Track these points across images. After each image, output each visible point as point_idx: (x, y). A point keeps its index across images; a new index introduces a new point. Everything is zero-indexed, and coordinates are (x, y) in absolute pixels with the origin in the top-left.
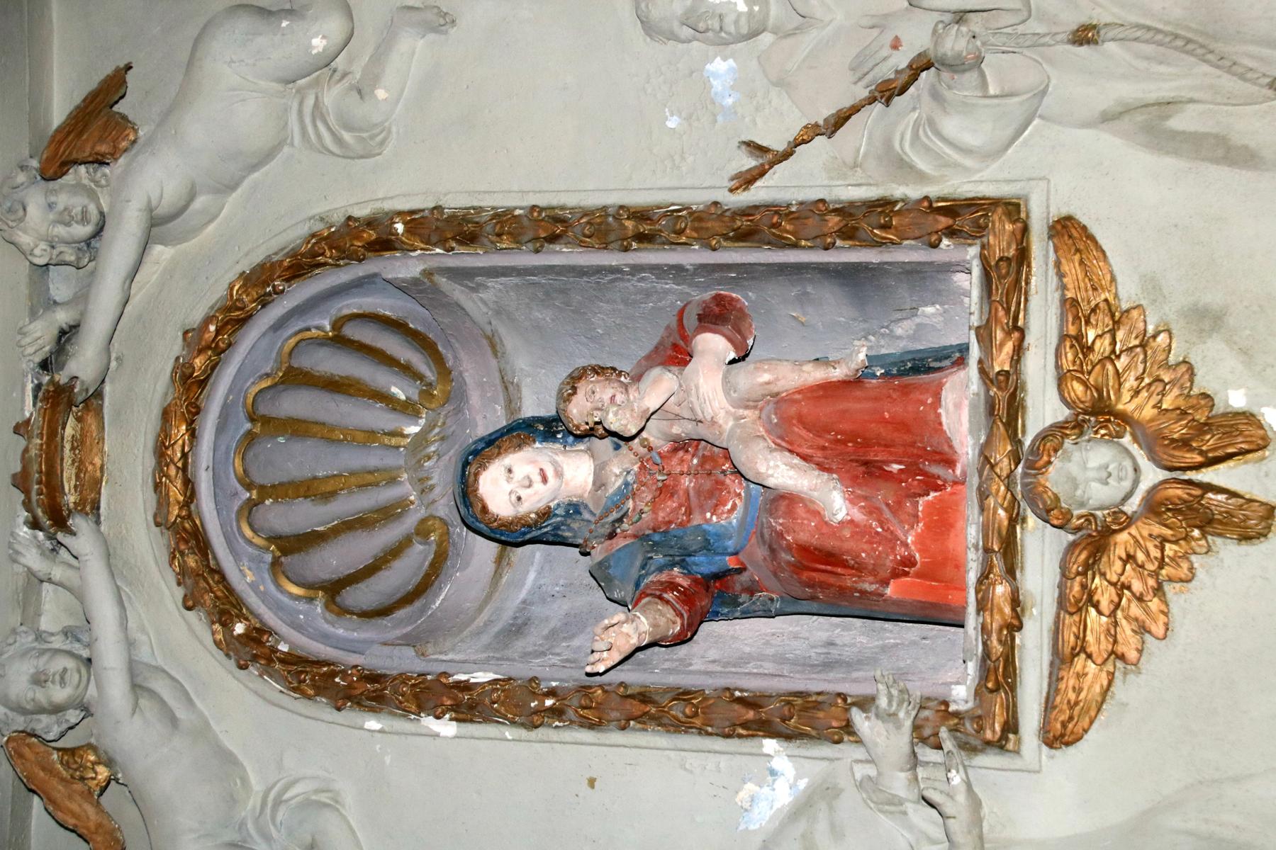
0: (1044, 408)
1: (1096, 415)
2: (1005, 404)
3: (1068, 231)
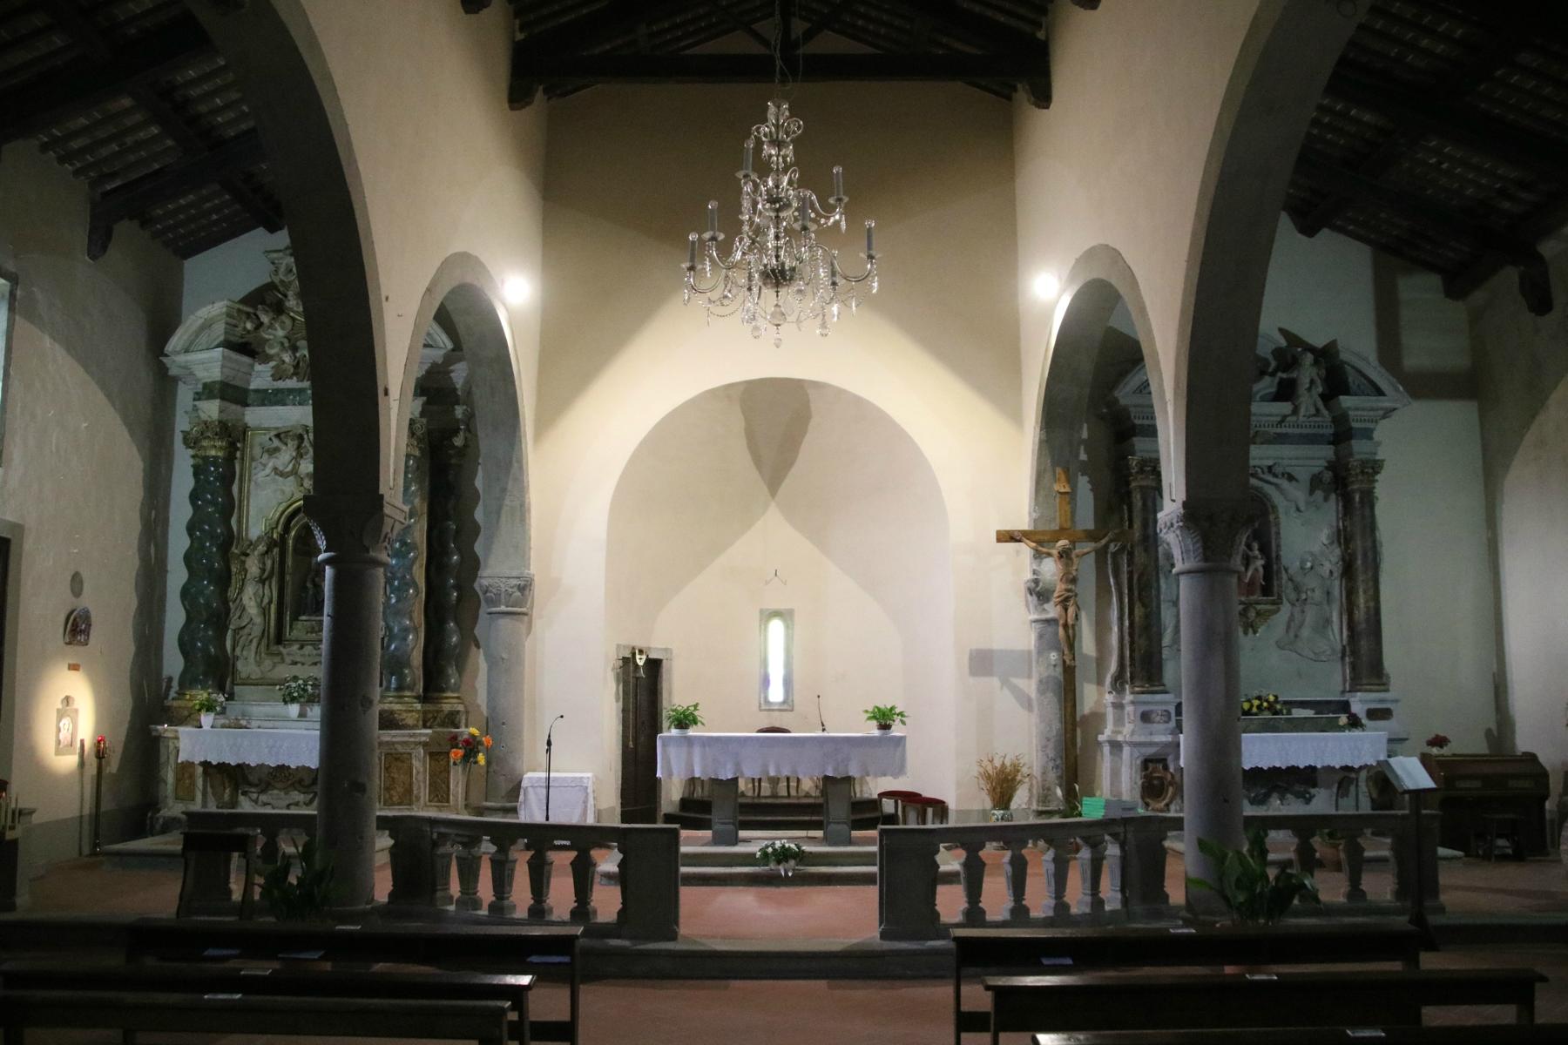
1: (1258, 614)
2: (1258, 603)
3: (1278, 611)
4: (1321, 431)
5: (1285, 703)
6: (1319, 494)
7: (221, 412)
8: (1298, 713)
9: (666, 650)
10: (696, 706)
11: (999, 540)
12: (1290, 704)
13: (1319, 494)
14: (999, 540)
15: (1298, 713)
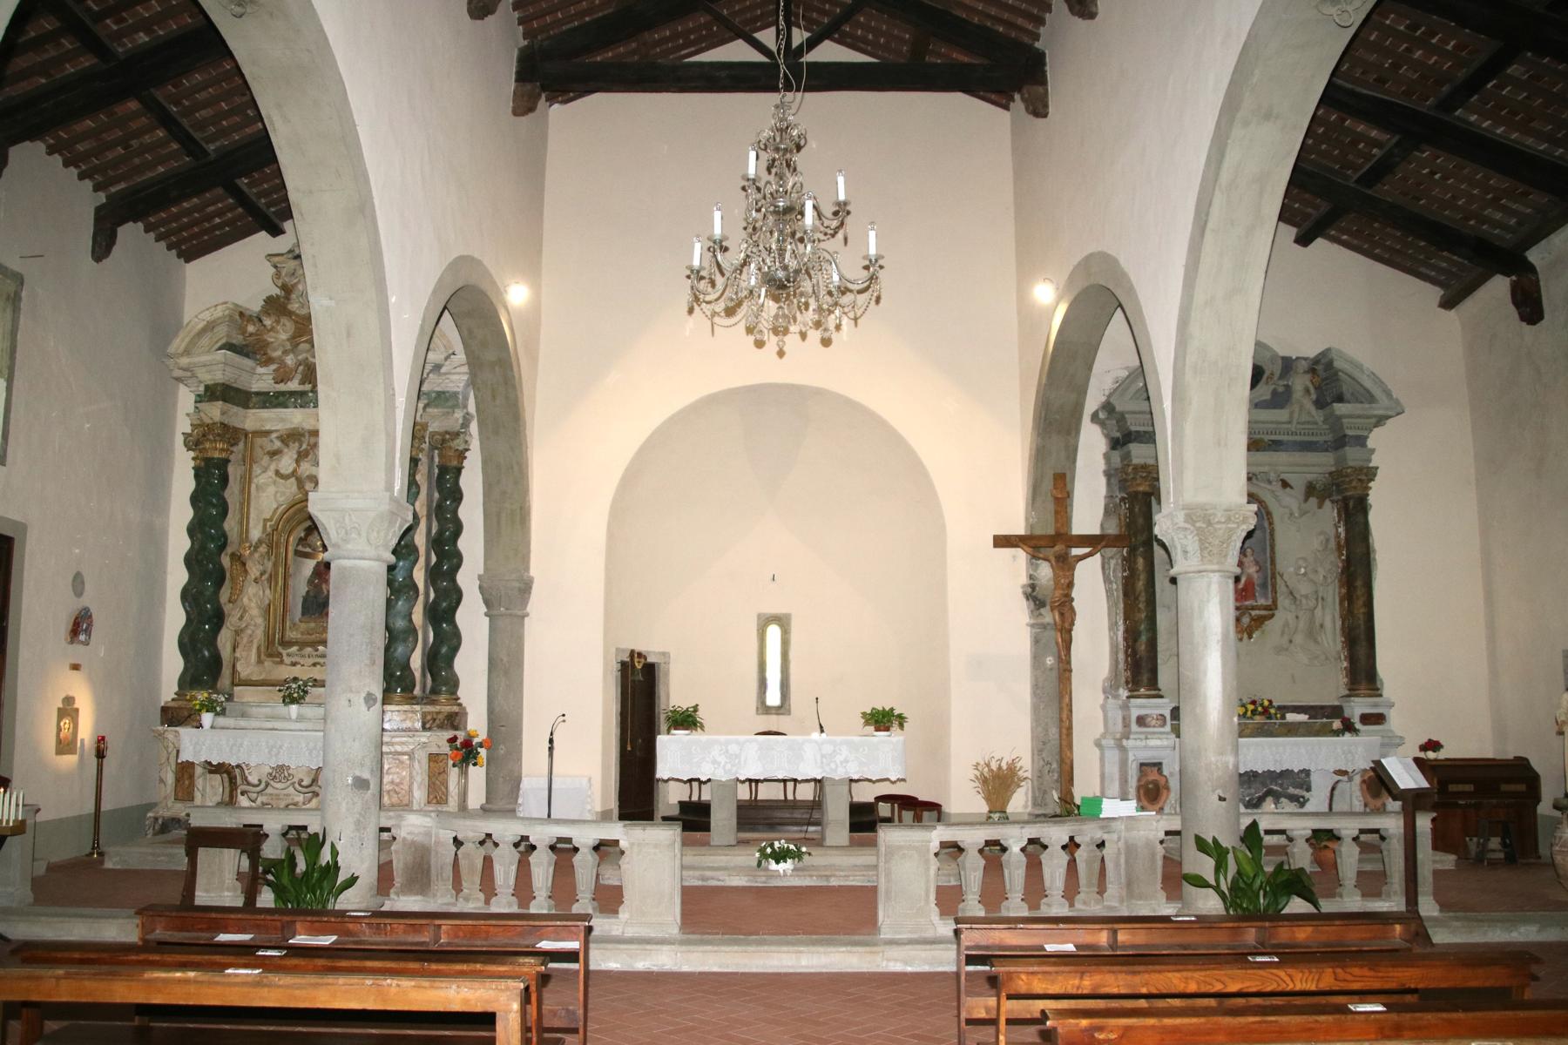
0: (1253, 613)
2: (1253, 608)
4: (1314, 439)
5: (1279, 708)
6: (1313, 501)
7: (223, 413)
8: (1291, 717)
9: (664, 654)
10: (696, 708)
11: (996, 545)
12: (1284, 709)
13: (1313, 501)
14: (996, 545)
15: (1291, 717)
